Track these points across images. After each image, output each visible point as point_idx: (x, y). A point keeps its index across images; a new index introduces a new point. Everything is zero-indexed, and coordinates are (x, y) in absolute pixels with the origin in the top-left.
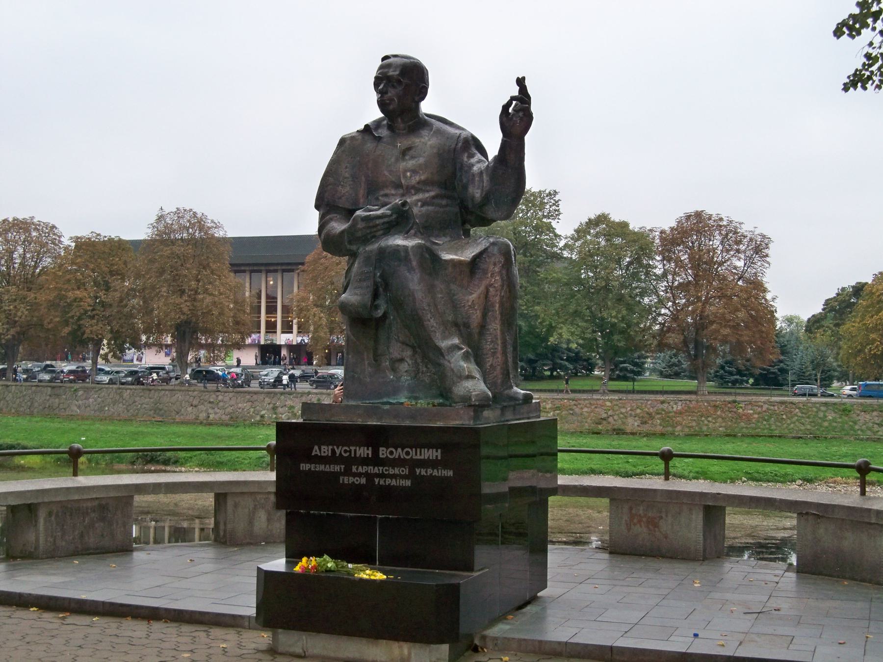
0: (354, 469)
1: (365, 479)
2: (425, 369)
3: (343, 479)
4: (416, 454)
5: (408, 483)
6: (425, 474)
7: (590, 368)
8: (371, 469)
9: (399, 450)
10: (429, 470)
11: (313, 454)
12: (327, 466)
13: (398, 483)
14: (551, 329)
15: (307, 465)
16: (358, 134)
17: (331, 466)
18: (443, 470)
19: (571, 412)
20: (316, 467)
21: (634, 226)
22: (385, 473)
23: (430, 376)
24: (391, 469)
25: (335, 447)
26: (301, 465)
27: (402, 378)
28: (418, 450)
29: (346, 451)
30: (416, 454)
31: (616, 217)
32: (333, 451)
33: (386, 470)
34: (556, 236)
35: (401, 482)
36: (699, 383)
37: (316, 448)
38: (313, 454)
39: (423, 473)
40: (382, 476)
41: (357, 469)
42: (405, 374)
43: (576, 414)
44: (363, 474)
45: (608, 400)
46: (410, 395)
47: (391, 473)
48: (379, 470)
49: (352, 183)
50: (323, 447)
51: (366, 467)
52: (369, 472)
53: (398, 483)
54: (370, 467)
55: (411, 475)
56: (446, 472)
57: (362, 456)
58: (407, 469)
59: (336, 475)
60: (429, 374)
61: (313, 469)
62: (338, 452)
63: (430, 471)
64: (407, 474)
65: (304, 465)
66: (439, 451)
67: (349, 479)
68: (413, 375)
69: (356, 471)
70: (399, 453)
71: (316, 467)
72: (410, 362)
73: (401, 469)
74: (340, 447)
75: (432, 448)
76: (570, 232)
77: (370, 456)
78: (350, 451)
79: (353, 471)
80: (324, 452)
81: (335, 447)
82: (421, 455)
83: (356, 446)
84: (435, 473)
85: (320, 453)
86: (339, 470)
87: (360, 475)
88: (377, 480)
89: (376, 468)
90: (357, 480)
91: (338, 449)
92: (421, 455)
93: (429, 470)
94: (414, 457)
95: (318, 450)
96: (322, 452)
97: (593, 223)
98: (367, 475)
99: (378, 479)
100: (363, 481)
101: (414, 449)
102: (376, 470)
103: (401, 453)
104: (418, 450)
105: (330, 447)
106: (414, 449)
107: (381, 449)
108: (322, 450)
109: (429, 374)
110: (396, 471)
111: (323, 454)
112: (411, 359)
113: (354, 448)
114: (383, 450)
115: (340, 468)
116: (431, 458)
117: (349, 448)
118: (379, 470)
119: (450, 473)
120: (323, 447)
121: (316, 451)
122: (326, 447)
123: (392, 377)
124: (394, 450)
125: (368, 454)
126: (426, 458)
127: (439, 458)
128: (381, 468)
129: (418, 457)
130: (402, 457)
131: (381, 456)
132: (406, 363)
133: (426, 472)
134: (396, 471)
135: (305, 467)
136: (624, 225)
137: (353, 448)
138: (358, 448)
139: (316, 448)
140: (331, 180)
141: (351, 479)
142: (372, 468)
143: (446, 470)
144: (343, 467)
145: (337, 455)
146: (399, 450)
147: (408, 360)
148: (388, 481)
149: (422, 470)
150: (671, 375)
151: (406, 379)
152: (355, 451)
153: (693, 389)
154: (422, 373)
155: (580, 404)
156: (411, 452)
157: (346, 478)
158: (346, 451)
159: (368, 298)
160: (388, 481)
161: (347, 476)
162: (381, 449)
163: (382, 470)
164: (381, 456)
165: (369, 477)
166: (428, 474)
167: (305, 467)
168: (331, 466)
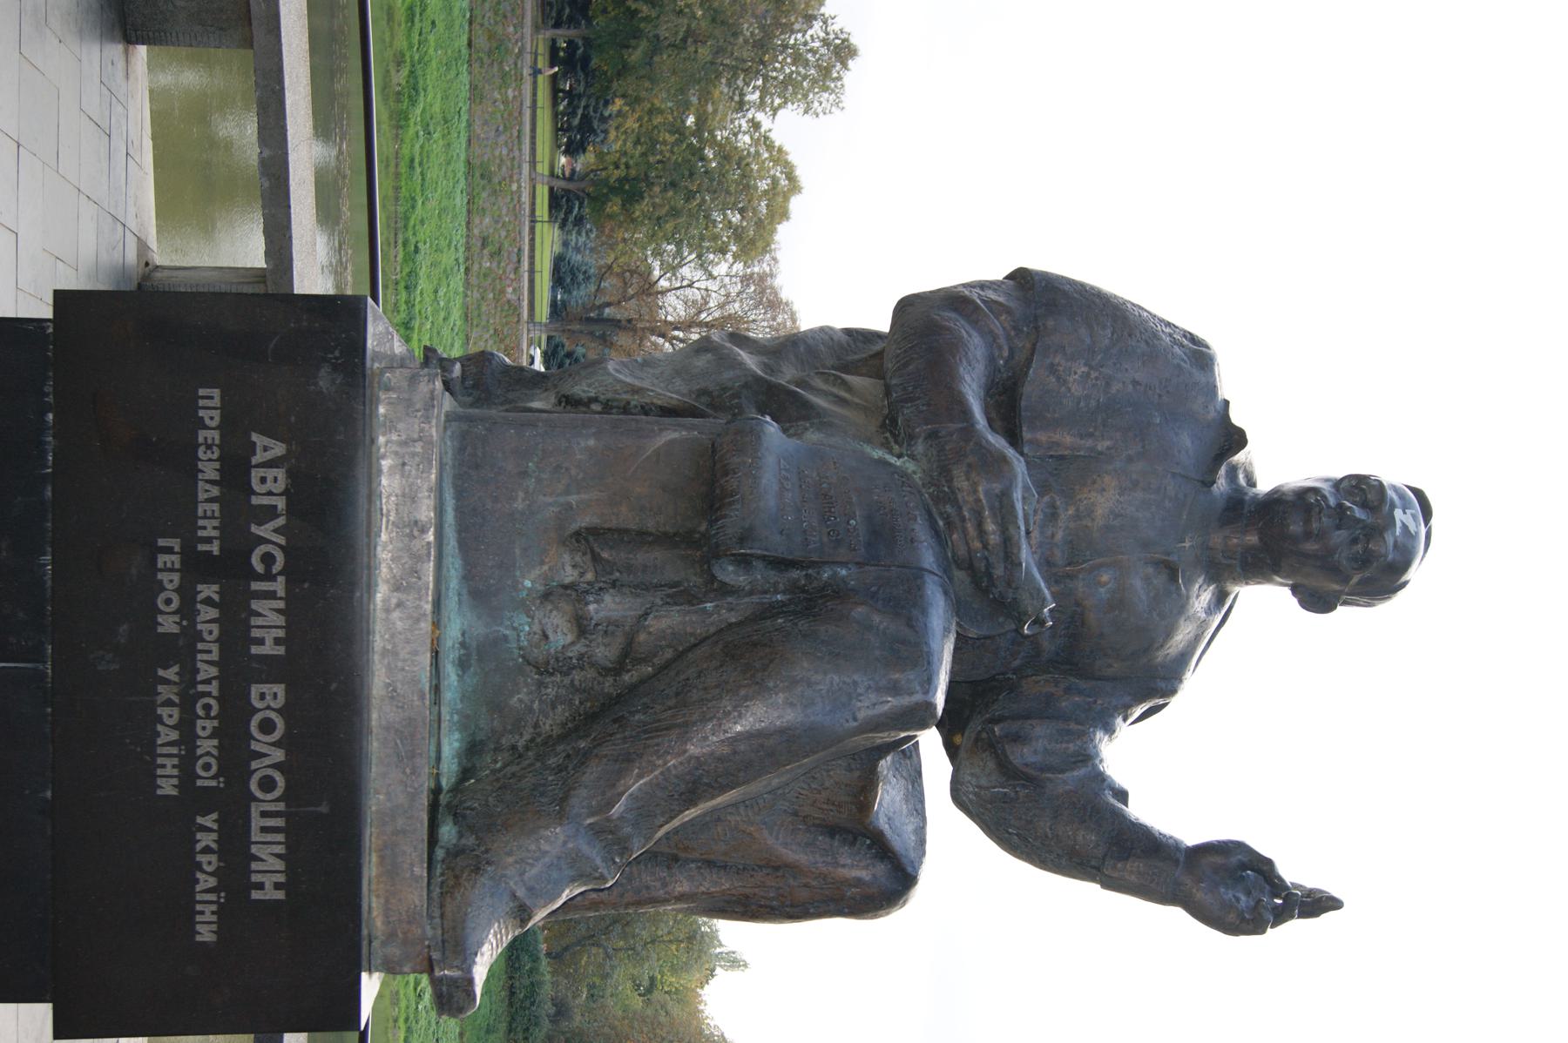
0: (209, 590)
1: (175, 629)
2: (551, 691)
3: (169, 550)
4: (264, 814)
5: (167, 788)
6: (199, 847)
7: (572, 150)
8: (209, 653)
9: (278, 755)
10: (214, 858)
11: (255, 437)
12: (215, 491)
13: (165, 750)
14: (634, 101)
15: (216, 414)
16: (1219, 406)
17: (216, 507)
18: (214, 908)
19: (501, 128)
20: (209, 447)
21: (783, 232)
22: (199, 705)
23: (531, 710)
24: (210, 725)
25: (281, 521)
26: (216, 393)
27: (524, 619)
28: (279, 822)
29: (268, 559)
30: (264, 814)
31: (795, 203)
32: (270, 513)
33: (207, 707)
34: (775, 111)
35: (169, 762)
36: (546, 325)
37: (279, 449)
38: (255, 437)
39: (206, 840)
40: (188, 702)
41: (208, 601)
42: (536, 628)
43: (498, 136)
44: (193, 623)
45: (519, 187)
46: (474, 644)
47: (200, 723)
48: (208, 682)
49: (1093, 403)
50: (280, 473)
51: (216, 633)
52: (200, 646)
53: (165, 750)
54: (215, 648)
55: (193, 798)
56: (208, 917)
57: (255, 621)
58: (213, 783)
59: (186, 525)
60: (536, 705)
61: (202, 435)
62: (264, 531)
63: (209, 862)
64: (199, 783)
65: (217, 402)
66: (280, 895)
67: (172, 570)
68: (537, 654)
69: (200, 597)
70: (268, 752)
71: (209, 447)
72: (572, 653)
73: (213, 761)
74: (281, 540)
75: (289, 871)
76: (778, 138)
77: (255, 650)
78: (269, 576)
79: (200, 587)
80: (263, 480)
81: (281, 521)
82: (264, 830)
83: (288, 599)
84: (206, 881)
85: (257, 466)
86: (201, 533)
87: (187, 610)
88: (171, 673)
89: (214, 671)
90: (168, 602)
91: (276, 531)
92: (264, 830)
93: (214, 858)
94: (255, 810)
95: (269, 455)
96: (261, 472)
97: (791, 177)
98: (192, 636)
99: (176, 679)
100: (168, 624)
101: (281, 806)
102: (207, 671)
103: (267, 761)
104: (279, 822)
105: (281, 503)
106: (281, 806)
107: (280, 689)
108: (271, 473)
109: (536, 705)
110: (207, 745)
111: (256, 475)
112: (581, 657)
113: (281, 593)
114: (275, 696)
115: (209, 540)
116: (254, 866)
117: (280, 573)
118: (208, 682)
119: (206, 933)
120: (280, 473)
121: (267, 448)
122: (280, 486)
123: (528, 584)
124: (277, 735)
125: (261, 642)
126: (254, 849)
127: (256, 895)
128: (214, 688)
129: (257, 822)
130: (254, 765)
131: (255, 690)
132: (570, 638)
133: (207, 850)
134: (207, 745)
135: (210, 404)
136: (784, 215)
137: (279, 586)
138: (281, 605)
139: (279, 449)
140: (1105, 336)
141: (171, 580)
142: (215, 656)
143: (214, 918)
144: (215, 548)
145: (254, 529)
146: (278, 755)
147: (580, 648)
148: (170, 715)
149: (214, 836)
150: (559, 272)
151: (521, 628)
152: (271, 595)
153: (537, 319)
154: (541, 685)
155: (512, 142)
156: (269, 797)
157: (176, 559)
158: (268, 559)
159: (777, 544)
160: (170, 715)
161: (183, 562)
162: (280, 689)
163: (209, 694)
164: (255, 690)
165: (183, 648)
166: (199, 858)
167: (210, 404)
168: (216, 507)
